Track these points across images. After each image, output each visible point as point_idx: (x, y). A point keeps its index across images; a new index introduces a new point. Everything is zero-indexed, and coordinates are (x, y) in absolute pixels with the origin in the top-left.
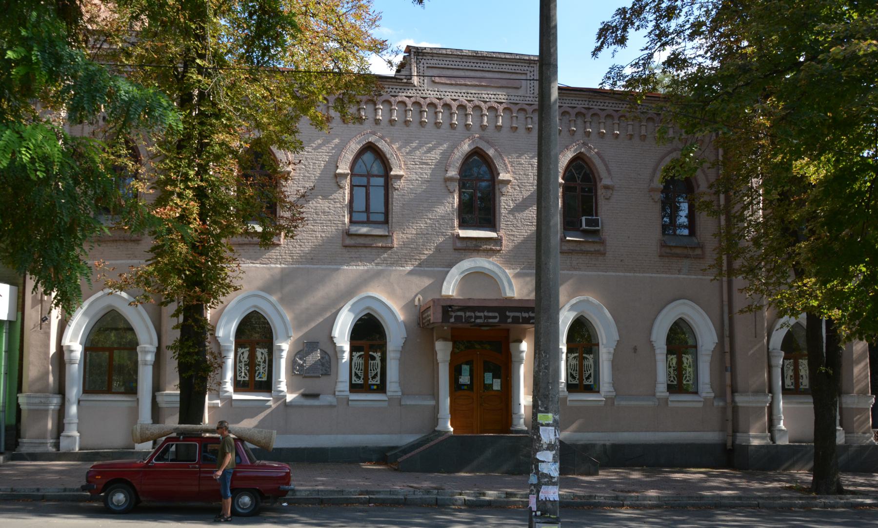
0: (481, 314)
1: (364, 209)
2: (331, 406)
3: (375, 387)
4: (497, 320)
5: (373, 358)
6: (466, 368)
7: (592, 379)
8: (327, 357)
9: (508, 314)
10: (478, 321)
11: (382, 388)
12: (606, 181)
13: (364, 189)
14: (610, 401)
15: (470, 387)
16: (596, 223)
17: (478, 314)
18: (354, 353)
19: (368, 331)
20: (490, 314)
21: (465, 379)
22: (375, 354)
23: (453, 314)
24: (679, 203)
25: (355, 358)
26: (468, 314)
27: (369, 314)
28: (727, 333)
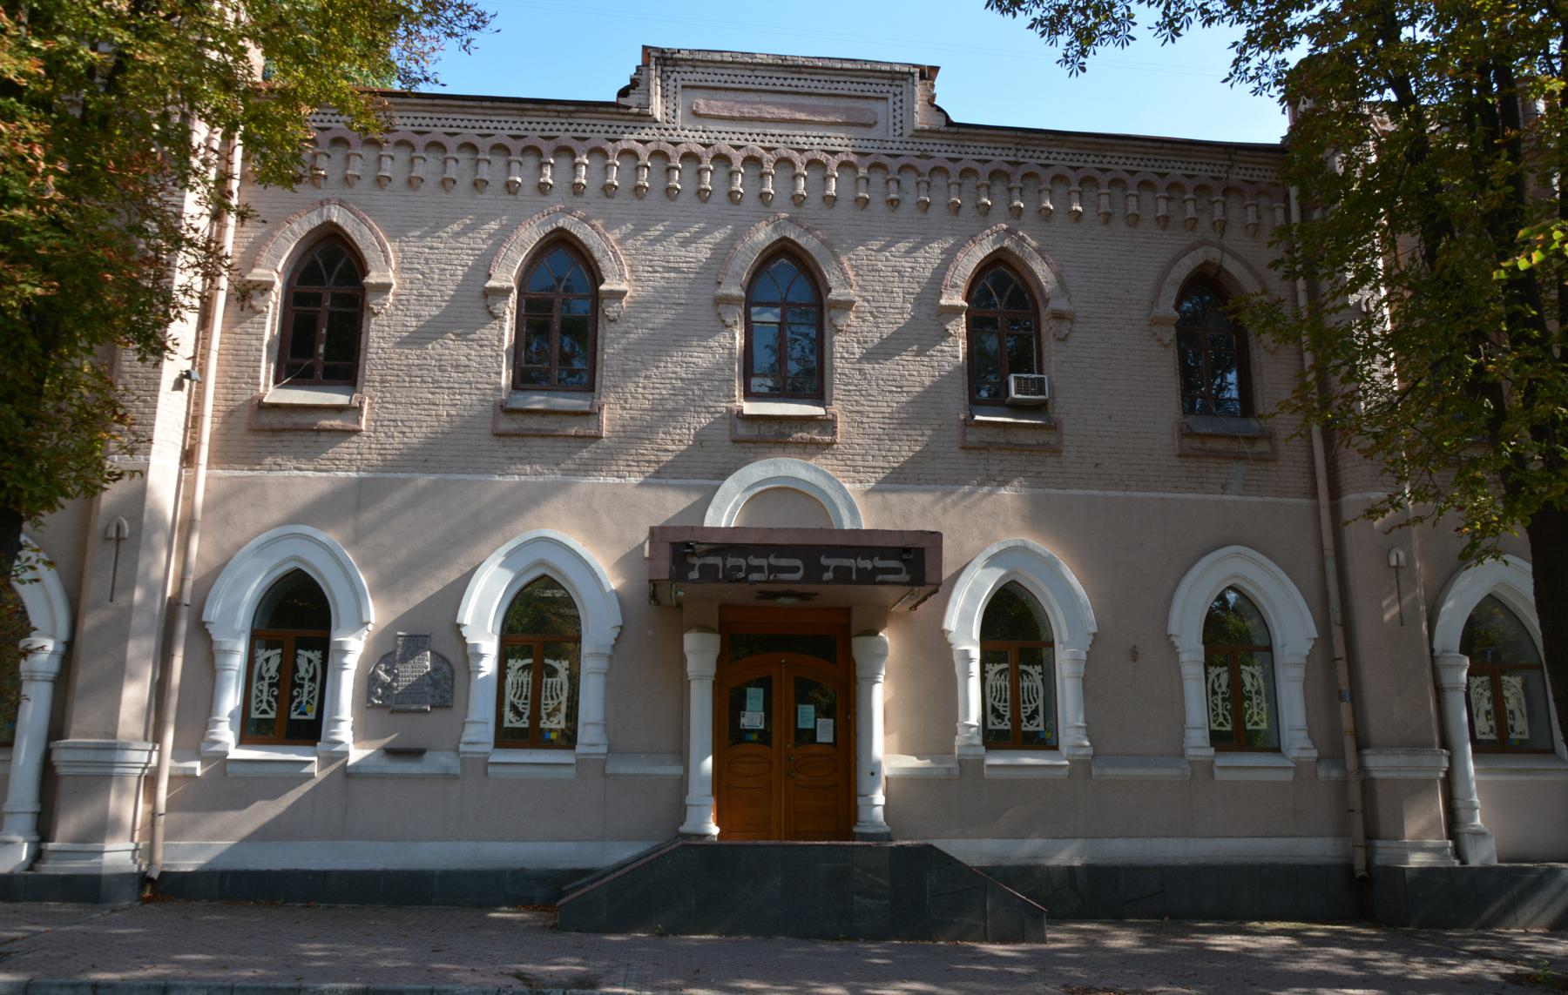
0: (763, 562)
2: (448, 777)
4: (798, 576)
5: (553, 672)
6: (755, 696)
9: (824, 561)
11: (568, 739)
15: (764, 736)
17: (754, 562)
18: (989, 666)
20: (784, 562)
21: (752, 718)
22: (556, 664)
23: (697, 562)
25: (990, 676)
26: (732, 561)
28: (1336, 616)
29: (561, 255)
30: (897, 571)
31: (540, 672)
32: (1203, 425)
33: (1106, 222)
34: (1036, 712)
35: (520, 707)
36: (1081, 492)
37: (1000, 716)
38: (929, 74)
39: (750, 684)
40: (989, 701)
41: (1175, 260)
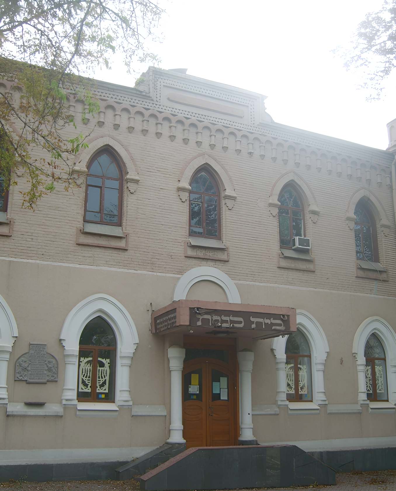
0: (227, 318)
1: (98, 210)
2: (58, 417)
3: (103, 396)
5: (102, 365)
6: (195, 378)
7: (305, 389)
8: (54, 361)
9: (252, 319)
10: (224, 325)
11: (110, 397)
12: (313, 207)
13: (99, 189)
14: (324, 406)
15: (199, 397)
16: (307, 242)
17: (224, 318)
18: (82, 359)
19: (98, 338)
21: (194, 389)
22: (104, 361)
23: (201, 317)
24: (6, 40)
25: (82, 364)
26: (215, 318)
27: (99, 317)
29: (104, 159)
30: (280, 325)
31: (96, 364)
32: (289, 253)
33: (329, 174)
34: (105, 383)
35: (87, 382)
36: (322, 290)
37: (86, 385)
38: (186, 70)
39: (194, 372)
40: (81, 376)
41: (195, 158)
